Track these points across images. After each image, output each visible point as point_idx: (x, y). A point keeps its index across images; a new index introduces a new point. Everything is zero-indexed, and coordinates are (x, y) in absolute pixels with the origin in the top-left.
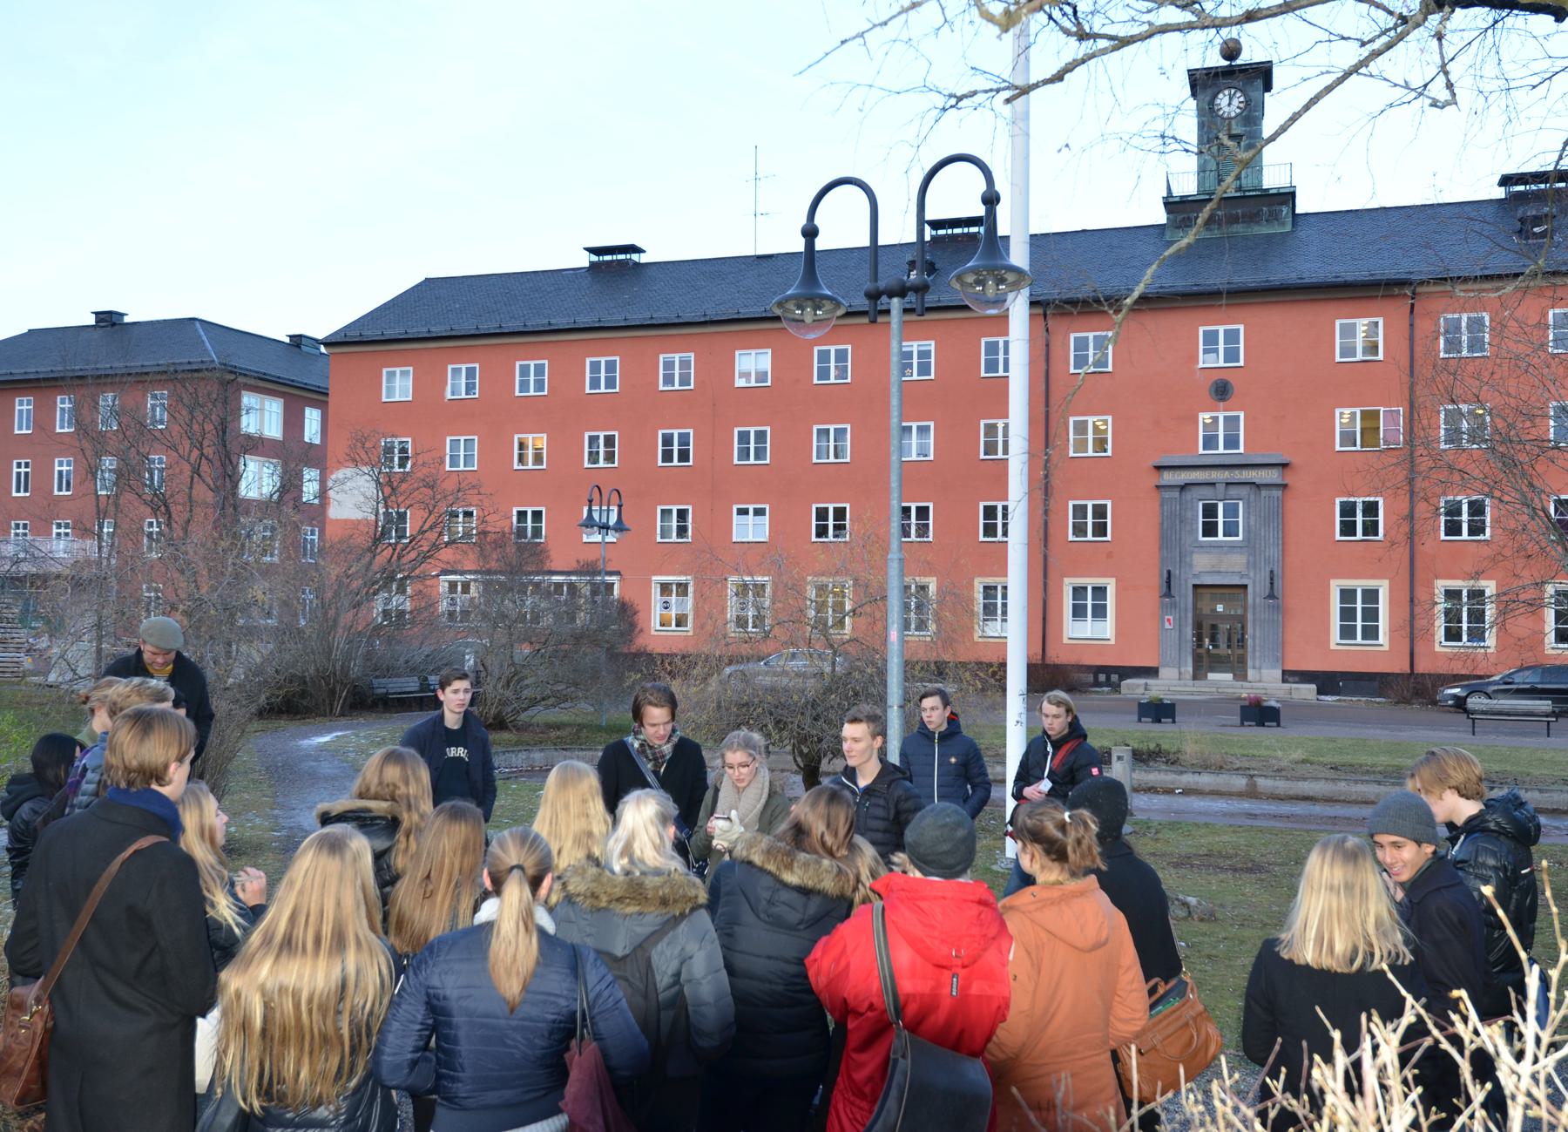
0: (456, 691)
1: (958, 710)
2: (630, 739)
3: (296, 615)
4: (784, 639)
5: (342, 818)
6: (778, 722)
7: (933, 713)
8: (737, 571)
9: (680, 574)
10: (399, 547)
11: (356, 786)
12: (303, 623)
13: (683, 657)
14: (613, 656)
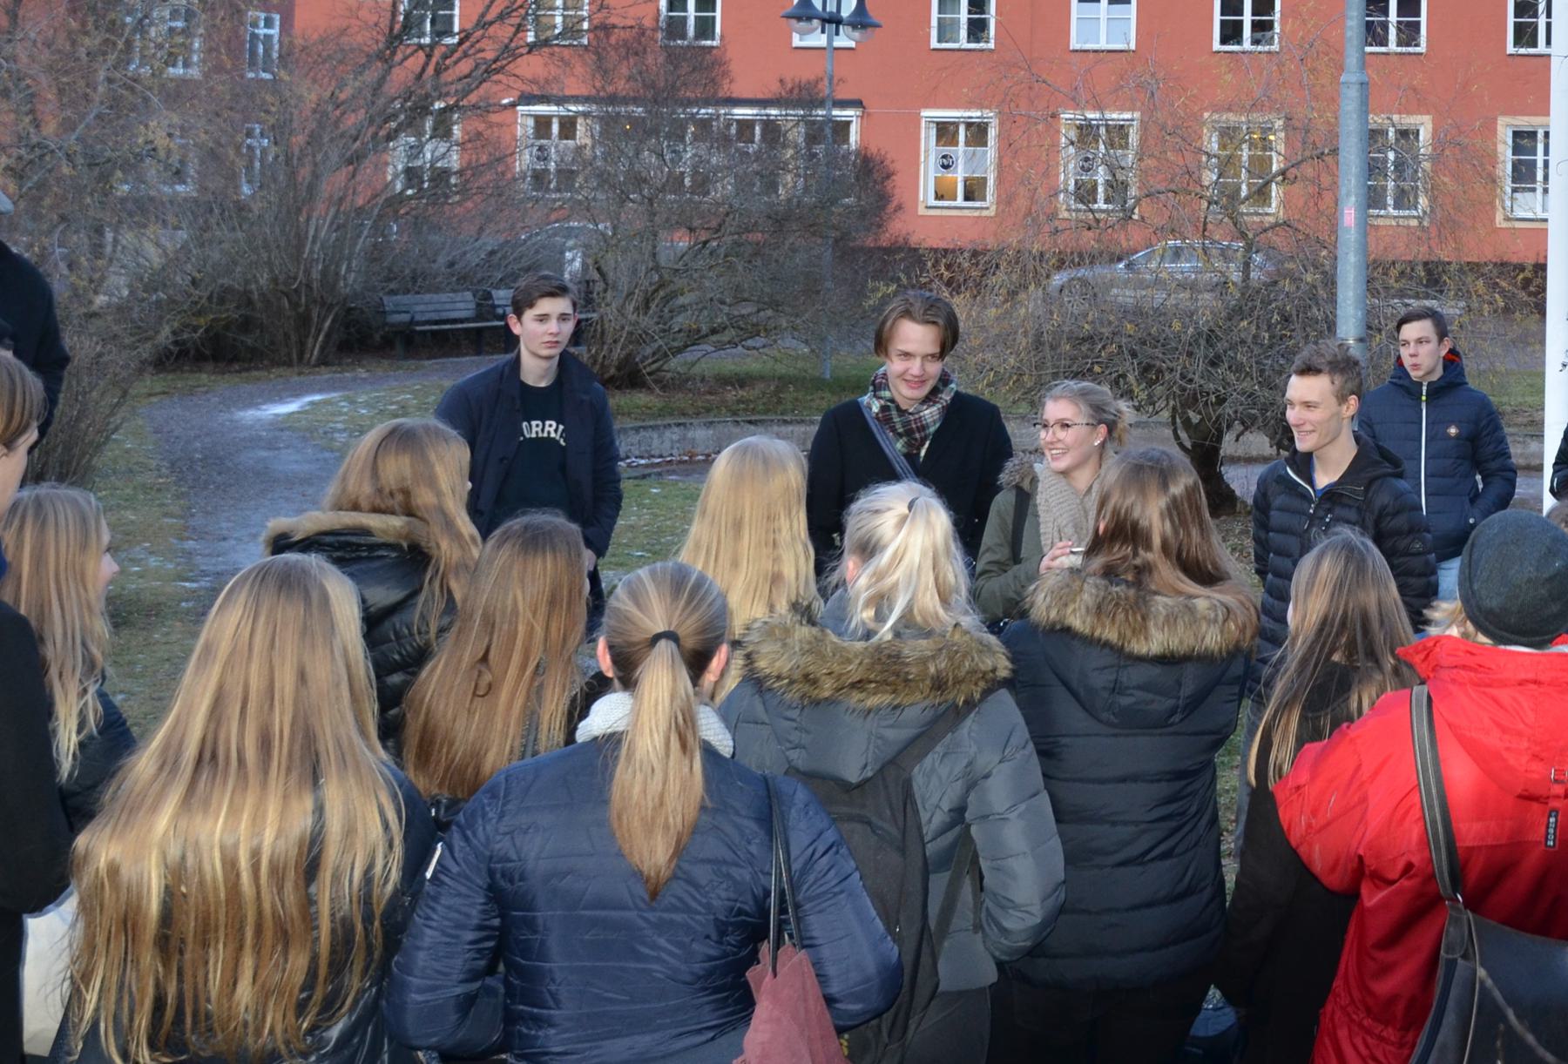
0: (543, 318)
1: (1463, 347)
2: (865, 399)
3: (232, 177)
4: (1158, 221)
5: (309, 544)
6: (1146, 369)
7: (1420, 350)
8: (1076, 104)
9: (970, 105)
10: (437, 53)
11: (332, 490)
12: (246, 190)
13: (975, 254)
14: (845, 251)
